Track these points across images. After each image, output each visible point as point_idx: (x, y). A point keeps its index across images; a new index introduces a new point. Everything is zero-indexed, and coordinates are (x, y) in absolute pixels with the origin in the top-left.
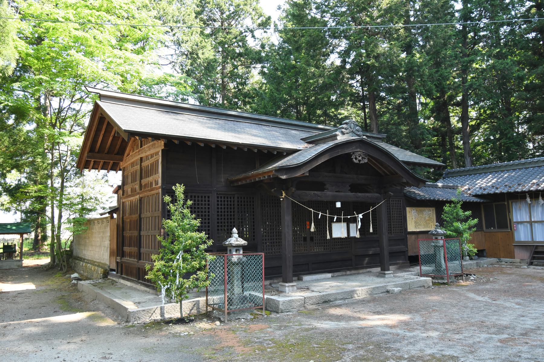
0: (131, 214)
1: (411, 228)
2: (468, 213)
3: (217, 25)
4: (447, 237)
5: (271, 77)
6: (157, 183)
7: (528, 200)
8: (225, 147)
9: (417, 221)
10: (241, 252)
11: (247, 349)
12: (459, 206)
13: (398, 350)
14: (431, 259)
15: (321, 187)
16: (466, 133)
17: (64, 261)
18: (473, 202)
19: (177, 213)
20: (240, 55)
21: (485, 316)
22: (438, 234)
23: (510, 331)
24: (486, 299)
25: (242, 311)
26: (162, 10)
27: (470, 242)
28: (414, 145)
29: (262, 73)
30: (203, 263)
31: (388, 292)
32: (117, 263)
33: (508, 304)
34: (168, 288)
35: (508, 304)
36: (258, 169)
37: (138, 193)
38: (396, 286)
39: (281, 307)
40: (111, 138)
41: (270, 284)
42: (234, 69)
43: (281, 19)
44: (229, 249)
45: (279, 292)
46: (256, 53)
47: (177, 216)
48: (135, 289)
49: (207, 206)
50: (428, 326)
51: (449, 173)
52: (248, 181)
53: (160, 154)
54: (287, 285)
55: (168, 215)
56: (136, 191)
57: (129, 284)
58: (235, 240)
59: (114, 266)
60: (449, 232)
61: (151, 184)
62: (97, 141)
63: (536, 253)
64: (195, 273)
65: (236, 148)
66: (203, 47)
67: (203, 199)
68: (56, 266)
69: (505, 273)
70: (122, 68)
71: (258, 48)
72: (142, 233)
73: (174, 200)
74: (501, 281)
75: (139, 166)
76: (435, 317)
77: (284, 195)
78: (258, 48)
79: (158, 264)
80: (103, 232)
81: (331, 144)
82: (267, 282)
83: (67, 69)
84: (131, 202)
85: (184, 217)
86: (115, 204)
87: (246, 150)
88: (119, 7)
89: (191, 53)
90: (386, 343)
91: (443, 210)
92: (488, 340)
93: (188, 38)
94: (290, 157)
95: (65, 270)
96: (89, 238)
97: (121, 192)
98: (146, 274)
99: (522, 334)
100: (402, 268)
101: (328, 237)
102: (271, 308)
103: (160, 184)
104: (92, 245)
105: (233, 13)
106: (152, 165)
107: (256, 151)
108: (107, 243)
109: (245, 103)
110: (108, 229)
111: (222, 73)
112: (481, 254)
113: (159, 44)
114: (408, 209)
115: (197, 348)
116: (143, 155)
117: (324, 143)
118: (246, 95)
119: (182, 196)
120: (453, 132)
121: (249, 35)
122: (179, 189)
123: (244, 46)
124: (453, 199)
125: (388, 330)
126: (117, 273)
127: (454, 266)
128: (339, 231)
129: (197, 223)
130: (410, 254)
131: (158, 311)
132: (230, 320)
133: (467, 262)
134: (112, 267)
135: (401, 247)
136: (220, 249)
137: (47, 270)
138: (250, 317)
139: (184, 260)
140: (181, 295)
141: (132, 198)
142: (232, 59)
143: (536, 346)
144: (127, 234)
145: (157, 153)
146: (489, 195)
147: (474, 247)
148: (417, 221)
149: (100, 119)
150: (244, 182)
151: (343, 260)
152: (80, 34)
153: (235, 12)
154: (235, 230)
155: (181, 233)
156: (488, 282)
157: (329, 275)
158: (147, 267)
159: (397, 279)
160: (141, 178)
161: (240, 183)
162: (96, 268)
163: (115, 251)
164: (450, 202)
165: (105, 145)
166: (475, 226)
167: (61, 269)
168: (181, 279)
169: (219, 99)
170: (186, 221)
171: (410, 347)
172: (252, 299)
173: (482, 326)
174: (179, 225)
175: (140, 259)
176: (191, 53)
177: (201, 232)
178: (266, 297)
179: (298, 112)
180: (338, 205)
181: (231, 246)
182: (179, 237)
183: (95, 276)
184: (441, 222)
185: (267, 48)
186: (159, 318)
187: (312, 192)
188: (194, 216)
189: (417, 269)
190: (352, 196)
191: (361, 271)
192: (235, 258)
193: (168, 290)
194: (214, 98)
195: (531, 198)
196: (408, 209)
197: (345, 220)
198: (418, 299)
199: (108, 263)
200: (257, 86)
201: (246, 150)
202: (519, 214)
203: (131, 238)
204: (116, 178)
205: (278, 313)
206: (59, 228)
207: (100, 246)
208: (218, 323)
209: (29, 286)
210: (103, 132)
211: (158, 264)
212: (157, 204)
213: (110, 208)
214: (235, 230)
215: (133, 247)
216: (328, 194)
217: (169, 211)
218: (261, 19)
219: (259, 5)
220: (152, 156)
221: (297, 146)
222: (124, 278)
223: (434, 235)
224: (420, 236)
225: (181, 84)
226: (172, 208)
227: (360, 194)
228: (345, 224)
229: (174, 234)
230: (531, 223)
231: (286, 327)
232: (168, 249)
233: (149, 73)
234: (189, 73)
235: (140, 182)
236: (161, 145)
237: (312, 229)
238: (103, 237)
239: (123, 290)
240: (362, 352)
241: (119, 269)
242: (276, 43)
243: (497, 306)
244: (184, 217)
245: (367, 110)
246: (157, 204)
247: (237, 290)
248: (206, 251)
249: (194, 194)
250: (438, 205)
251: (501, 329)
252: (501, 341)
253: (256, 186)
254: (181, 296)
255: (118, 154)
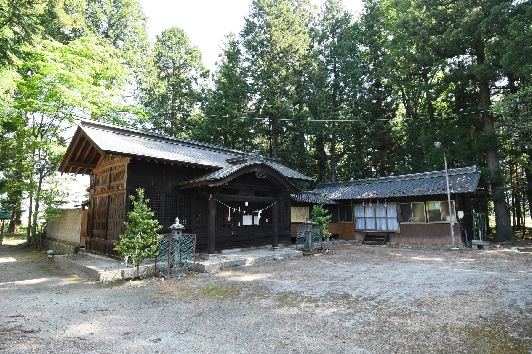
0: (100, 206)
1: (293, 220)
2: (327, 211)
3: (170, 71)
4: (314, 226)
5: (207, 111)
6: (123, 186)
7: (363, 204)
8: (173, 164)
9: (297, 216)
10: (181, 233)
11: (182, 293)
12: (322, 206)
13: (272, 290)
14: (304, 240)
15: (235, 192)
16: (336, 157)
17: (39, 241)
18: (332, 204)
19: (138, 207)
20: (186, 94)
21: (326, 272)
22: (308, 224)
23: (336, 279)
24: (331, 263)
25: (180, 271)
26: (129, 58)
27: (326, 229)
28: (301, 167)
29: (201, 108)
30: (155, 240)
31: (275, 259)
32: (87, 242)
33: (341, 266)
34: (130, 257)
35: (341, 266)
36: (195, 179)
37: (107, 192)
38: (280, 256)
39: (205, 269)
40: (88, 152)
41: (200, 256)
42: (181, 104)
43: (216, 72)
44: (172, 231)
45: (205, 260)
46: (198, 94)
47: (138, 209)
48: (102, 260)
49: (158, 203)
50: (293, 278)
51: (321, 185)
52: (188, 187)
53: (127, 166)
54: (210, 255)
55: (132, 208)
56: (105, 190)
57: (96, 256)
58: (177, 224)
59: (84, 244)
60: (314, 223)
61: (118, 186)
62: (77, 153)
63: (367, 236)
64: (149, 246)
65: (180, 165)
66: (159, 87)
67: (156, 198)
68: (32, 245)
69: (347, 249)
70: (96, 99)
71: (199, 91)
72: (109, 220)
73: (137, 199)
74: (344, 253)
75: (109, 173)
76: (299, 273)
77: (211, 196)
78: (199, 91)
79: (124, 241)
80: (76, 219)
81: (243, 165)
82: (198, 254)
83: (52, 96)
84: (101, 198)
85: (144, 209)
86: (87, 199)
87: (187, 166)
88: (96, 54)
89: (149, 91)
90: (266, 287)
91: (312, 209)
92: (323, 284)
93: (148, 79)
94: (217, 172)
95: (40, 248)
96: (62, 223)
97: (93, 190)
98: (115, 247)
99: (342, 280)
100: (286, 245)
101: (239, 225)
102: (200, 270)
103: (125, 187)
104: (64, 229)
105: (182, 65)
106: (119, 173)
107: (194, 167)
108: (79, 227)
109: (188, 129)
110: (81, 217)
111: (173, 107)
112: (334, 237)
113: (125, 82)
114: (292, 208)
115: (149, 293)
116: (113, 166)
117: (240, 164)
118: (189, 123)
119: (143, 196)
120: (326, 158)
121: (193, 82)
122: (141, 192)
123: (189, 88)
124: (319, 202)
125: (269, 280)
126: (87, 249)
127: (317, 245)
128: (247, 221)
129: (152, 214)
130: (292, 236)
131: (120, 273)
132: (172, 278)
133: (327, 242)
134: (82, 245)
135: (288, 232)
136: (166, 231)
137: (24, 248)
138: (184, 275)
139: (142, 238)
140: (138, 261)
141: (102, 195)
142: (180, 97)
143: (347, 286)
144: (96, 221)
145: (124, 166)
146: (342, 200)
147: (330, 232)
148: (297, 216)
149: (81, 139)
150: (185, 188)
151: (247, 240)
152: (66, 73)
153: (184, 65)
154: (177, 219)
155: (141, 220)
156: (336, 253)
157: (239, 250)
158: (115, 242)
159: (280, 252)
160: (110, 182)
161: (182, 188)
162: (68, 246)
163: (86, 233)
164: (316, 204)
165: (82, 156)
166: (330, 219)
167: (37, 247)
168: (139, 251)
169: (169, 124)
170: (144, 213)
171: (280, 288)
172: (186, 264)
173: (323, 277)
174: (139, 215)
175: (106, 238)
176: (150, 91)
177: (154, 220)
178: (196, 263)
179: (226, 138)
180: (247, 204)
181: (174, 229)
182: (139, 223)
183: (67, 252)
184: (311, 217)
185: (206, 92)
186: (121, 277)
187: (230, 196)
188: (150, 209)
189: (295, 246)
190: (255, 198)
191: (260, 247)
192: (177, 237)
193: (130, 258)
194: (166, 124)
195: (365, 203)
196: (292, 208)
197: (251, 214)
198: (292, 264)
199: (79, 242)
200: (197, 118)
201: (187, 166)
202: (358, 213)
203: (99, 223)
204: (85, 180)
205: (203, 273)
206: (36, 214)
207: (72, 229)
208: (163, 279)
209: (12, 260)
210: (82, 147)
211: (124, 241)
212: (122, 200)
213: (83, 202)
214: (177, 219)
215: (101, 232)
216: (241, 197)
217: (133, 206)
218: (202, 71)
219: (201, 61)
220: (120, 167)
221: (221, 164)
222: (92, 253)
223: (306, 224)
224: (299, 225)
225: (140, 112)
226: (135, 203)
227: (260, 198)
228: (251, 217)
229: (135, 221)
230: (365, 218)
231: (207, 280)
232: (131, 231)
233: (115, 102)
234: (147, 105)
235: (109, 184)
236: (127, 160)
237: (229, 220)
238: (75, 223)
239: (92, 261)
240: (251, 292)
241: (89, 246)
242: (213, 89)
243: (335, 266)
244: (144, 209)
245: (272, 140)
246: (122, 200)
247: (177, 258)
248: (158, 232)
249: (149, 194)
250: (310, 205)
251: (332, 278)
252: (330, 284)
253: (193, 190)
254: (139, 261)
255: (92, 163)
